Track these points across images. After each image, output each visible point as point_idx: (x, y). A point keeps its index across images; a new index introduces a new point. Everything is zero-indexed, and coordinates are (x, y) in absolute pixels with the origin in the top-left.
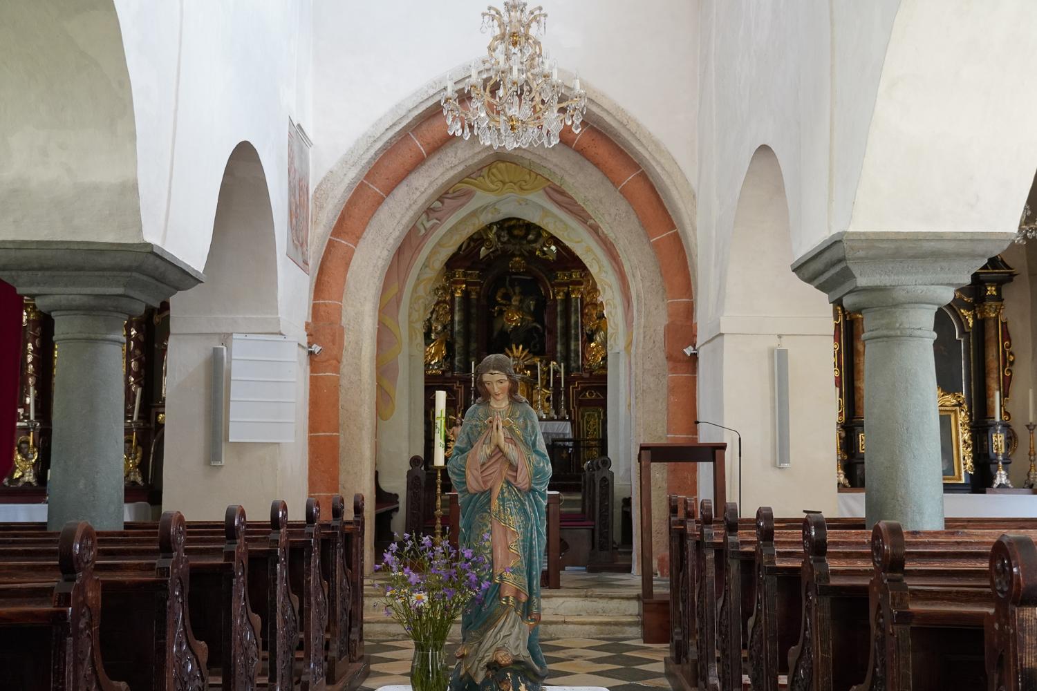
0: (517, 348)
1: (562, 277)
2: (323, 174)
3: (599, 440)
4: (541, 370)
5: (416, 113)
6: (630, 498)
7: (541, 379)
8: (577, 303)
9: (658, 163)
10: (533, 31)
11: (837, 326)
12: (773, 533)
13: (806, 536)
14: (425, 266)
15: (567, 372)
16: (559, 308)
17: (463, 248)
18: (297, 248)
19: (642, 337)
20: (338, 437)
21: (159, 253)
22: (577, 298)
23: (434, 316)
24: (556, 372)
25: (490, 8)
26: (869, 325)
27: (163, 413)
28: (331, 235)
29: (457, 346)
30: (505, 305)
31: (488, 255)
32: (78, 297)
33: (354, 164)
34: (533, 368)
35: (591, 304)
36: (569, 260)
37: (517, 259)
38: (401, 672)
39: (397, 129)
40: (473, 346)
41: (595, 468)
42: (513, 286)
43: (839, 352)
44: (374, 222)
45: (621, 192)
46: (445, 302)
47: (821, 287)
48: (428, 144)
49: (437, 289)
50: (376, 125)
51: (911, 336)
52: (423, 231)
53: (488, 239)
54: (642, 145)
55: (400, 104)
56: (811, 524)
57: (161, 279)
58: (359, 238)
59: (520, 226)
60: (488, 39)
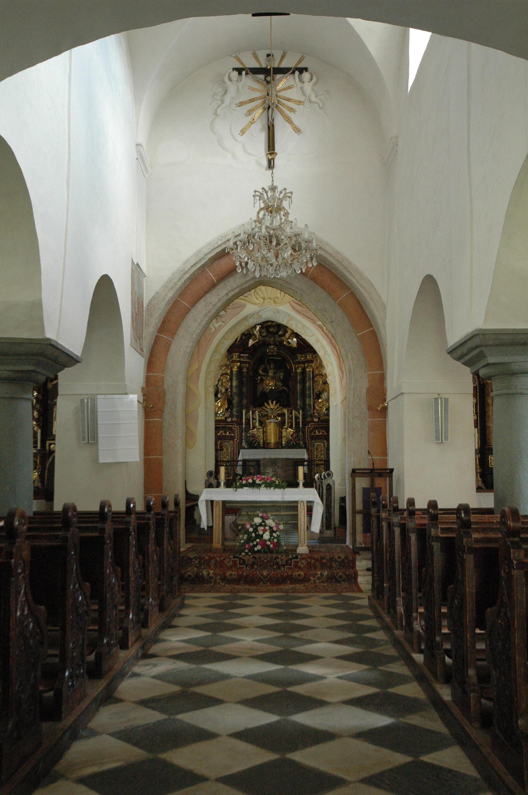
0: (272, 403)
1: (300, 358)
2: (152, 294)
3: (324, 461)
4: (288, 417)
5: (210, 256)
6: (345, 497)
7: (288, 422)
8: (310, 374)
9: (362, 286)
10: (285, 204)
11: (475, 388)
12: (438, 516)
13: (459, 518)
14: (215, 351)
15: (304, 418)
16: (299, 378)
17: (238, 340)
18: (136, 341)
19: (352, 395)
20: (162, 459)
21: (55, 344)
22: (310, 371)
23: (220, 383)
24: (297, 418)
25: (255, 191)
26: (496, 388)
27: (54, 444)
28: (157, 333)
29: (234, 401)
30: (264, 376)
31: (254, 344)
32: (5, 372)
33: (172, 288)
34: (282, 415)
35: (319, 375)
36: (305, 347)
37: (272, 347)
38: (208, 604)
39: (199, 266)
40: (245, 401)
41: (323, 478)
42: (269, 363)
43: (476, 404)
44: (184, 324)
45: (338, 304)
46: (226, 374)
47: (466, 364)
48: (218, 275)
49: (222, 366)
50: (185, 263)
51: (522, 394)
52: (213, 330)
53: (254, 334)
54: (352, 275)
55: (200, 250)
56: (464, 508)
57: (55, 360)
58: (174, 334)
59: (274, 326)
60: (257, 209)
